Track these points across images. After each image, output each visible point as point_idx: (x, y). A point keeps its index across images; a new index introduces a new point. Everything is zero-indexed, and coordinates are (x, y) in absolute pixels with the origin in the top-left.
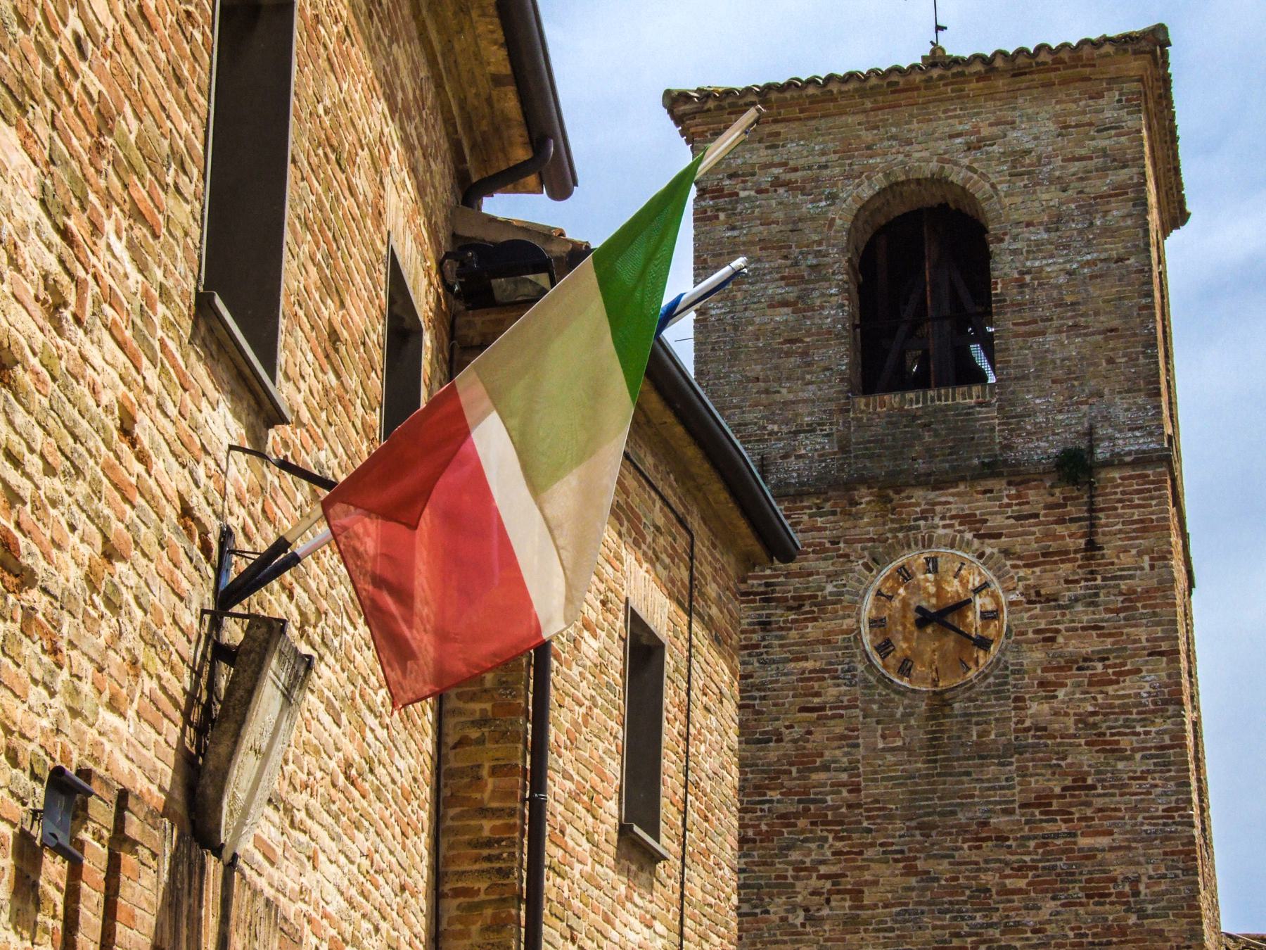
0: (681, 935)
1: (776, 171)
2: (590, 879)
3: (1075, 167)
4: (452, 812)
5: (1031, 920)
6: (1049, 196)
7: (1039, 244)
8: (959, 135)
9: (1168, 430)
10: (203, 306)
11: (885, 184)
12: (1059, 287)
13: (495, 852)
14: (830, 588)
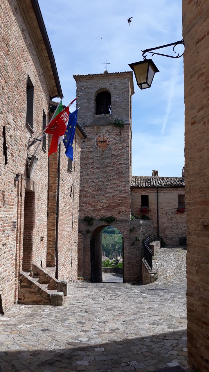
0: (74, 179)
1: (86, 86)
2: (64, 174)
3: (121, 88)
4: (50, 168)
5: (112, 175)
6: (118, 91)
7: (117, 97)
8: (108, 83)
9: (130, 120)
10: (26, 124)
11: (99, 89)
12: (118, 103)
13: (55, 172)
14: (91, 138)
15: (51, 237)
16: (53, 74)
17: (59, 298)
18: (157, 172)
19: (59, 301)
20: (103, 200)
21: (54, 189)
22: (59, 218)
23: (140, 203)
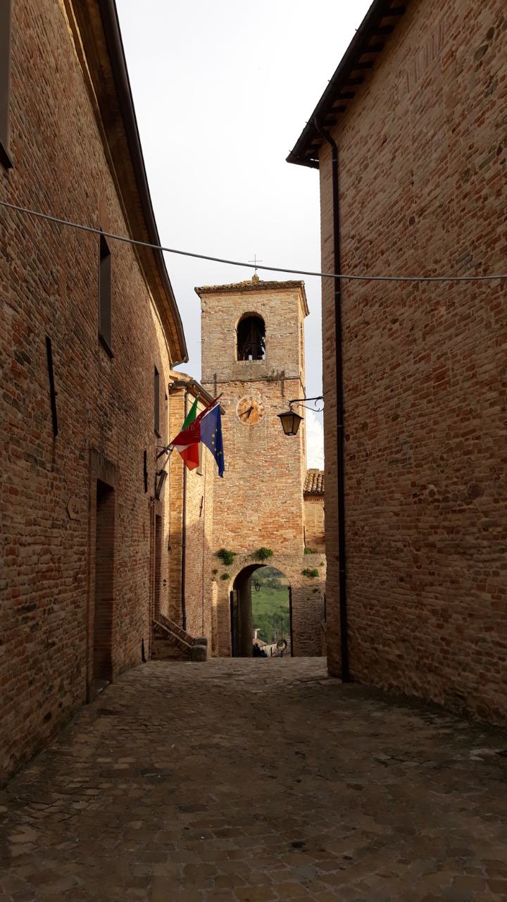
3: (283, 312)
5: (268, 471)
19: (202, 655)
22: (187, 552)
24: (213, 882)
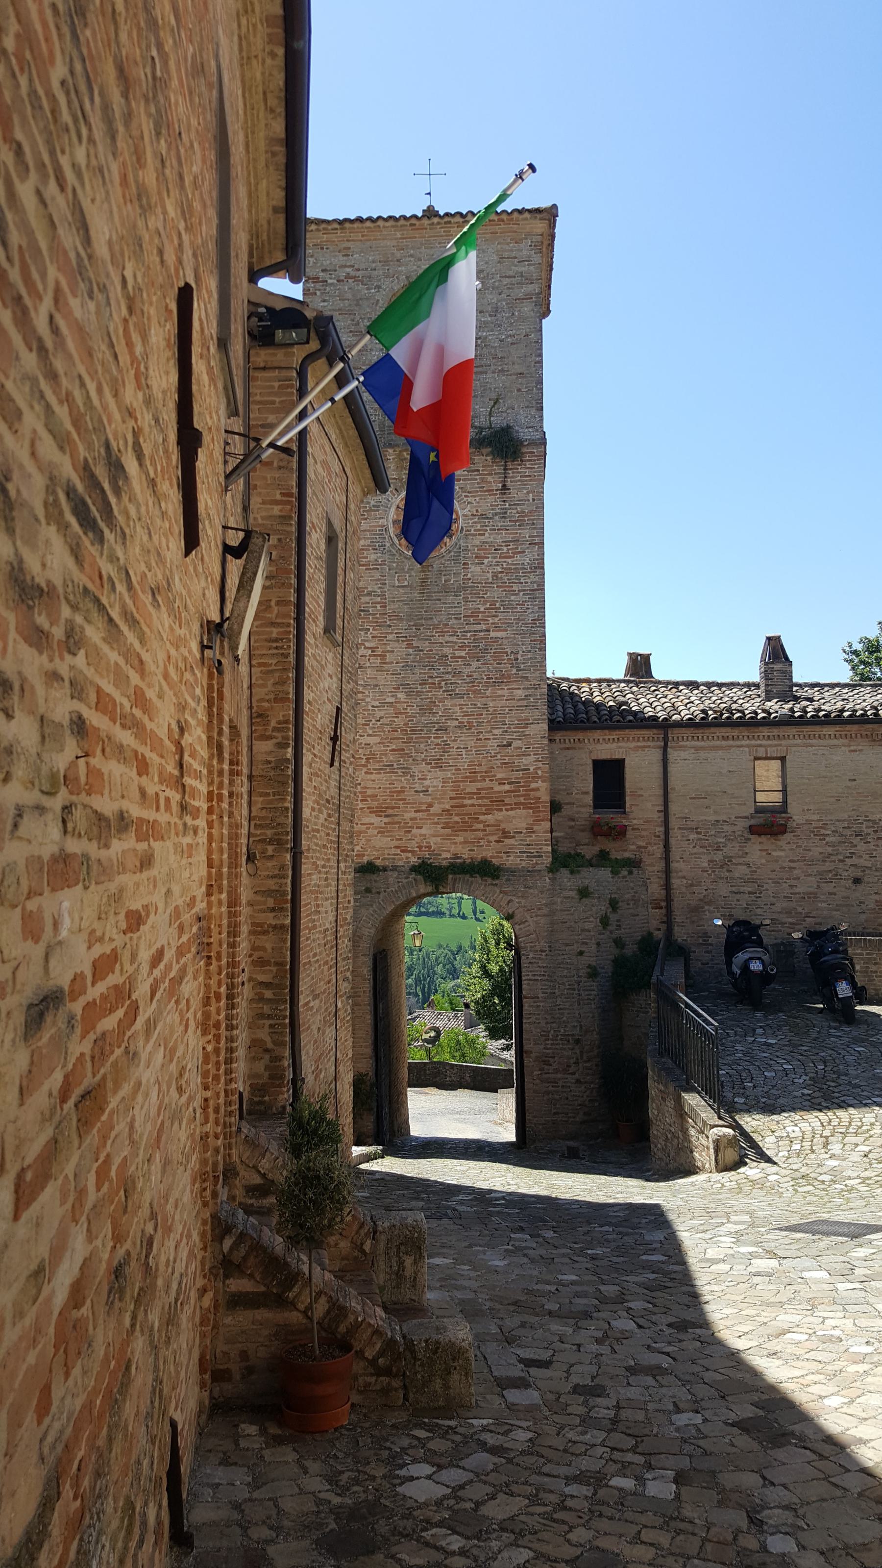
1: (348, 270)
3: (506, 281)
5: (466, 671)
11: (406, 283)
15: (268, 963)
16: (283, 136)
17: (454, 1359)
18: (646, 658)
20: (427, 783)
21: (275, 729)
23: (587, 793)
24: (189, 952)
